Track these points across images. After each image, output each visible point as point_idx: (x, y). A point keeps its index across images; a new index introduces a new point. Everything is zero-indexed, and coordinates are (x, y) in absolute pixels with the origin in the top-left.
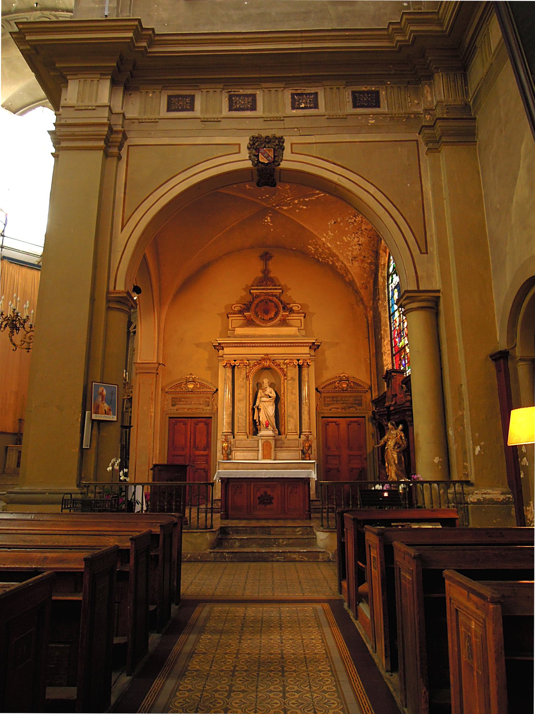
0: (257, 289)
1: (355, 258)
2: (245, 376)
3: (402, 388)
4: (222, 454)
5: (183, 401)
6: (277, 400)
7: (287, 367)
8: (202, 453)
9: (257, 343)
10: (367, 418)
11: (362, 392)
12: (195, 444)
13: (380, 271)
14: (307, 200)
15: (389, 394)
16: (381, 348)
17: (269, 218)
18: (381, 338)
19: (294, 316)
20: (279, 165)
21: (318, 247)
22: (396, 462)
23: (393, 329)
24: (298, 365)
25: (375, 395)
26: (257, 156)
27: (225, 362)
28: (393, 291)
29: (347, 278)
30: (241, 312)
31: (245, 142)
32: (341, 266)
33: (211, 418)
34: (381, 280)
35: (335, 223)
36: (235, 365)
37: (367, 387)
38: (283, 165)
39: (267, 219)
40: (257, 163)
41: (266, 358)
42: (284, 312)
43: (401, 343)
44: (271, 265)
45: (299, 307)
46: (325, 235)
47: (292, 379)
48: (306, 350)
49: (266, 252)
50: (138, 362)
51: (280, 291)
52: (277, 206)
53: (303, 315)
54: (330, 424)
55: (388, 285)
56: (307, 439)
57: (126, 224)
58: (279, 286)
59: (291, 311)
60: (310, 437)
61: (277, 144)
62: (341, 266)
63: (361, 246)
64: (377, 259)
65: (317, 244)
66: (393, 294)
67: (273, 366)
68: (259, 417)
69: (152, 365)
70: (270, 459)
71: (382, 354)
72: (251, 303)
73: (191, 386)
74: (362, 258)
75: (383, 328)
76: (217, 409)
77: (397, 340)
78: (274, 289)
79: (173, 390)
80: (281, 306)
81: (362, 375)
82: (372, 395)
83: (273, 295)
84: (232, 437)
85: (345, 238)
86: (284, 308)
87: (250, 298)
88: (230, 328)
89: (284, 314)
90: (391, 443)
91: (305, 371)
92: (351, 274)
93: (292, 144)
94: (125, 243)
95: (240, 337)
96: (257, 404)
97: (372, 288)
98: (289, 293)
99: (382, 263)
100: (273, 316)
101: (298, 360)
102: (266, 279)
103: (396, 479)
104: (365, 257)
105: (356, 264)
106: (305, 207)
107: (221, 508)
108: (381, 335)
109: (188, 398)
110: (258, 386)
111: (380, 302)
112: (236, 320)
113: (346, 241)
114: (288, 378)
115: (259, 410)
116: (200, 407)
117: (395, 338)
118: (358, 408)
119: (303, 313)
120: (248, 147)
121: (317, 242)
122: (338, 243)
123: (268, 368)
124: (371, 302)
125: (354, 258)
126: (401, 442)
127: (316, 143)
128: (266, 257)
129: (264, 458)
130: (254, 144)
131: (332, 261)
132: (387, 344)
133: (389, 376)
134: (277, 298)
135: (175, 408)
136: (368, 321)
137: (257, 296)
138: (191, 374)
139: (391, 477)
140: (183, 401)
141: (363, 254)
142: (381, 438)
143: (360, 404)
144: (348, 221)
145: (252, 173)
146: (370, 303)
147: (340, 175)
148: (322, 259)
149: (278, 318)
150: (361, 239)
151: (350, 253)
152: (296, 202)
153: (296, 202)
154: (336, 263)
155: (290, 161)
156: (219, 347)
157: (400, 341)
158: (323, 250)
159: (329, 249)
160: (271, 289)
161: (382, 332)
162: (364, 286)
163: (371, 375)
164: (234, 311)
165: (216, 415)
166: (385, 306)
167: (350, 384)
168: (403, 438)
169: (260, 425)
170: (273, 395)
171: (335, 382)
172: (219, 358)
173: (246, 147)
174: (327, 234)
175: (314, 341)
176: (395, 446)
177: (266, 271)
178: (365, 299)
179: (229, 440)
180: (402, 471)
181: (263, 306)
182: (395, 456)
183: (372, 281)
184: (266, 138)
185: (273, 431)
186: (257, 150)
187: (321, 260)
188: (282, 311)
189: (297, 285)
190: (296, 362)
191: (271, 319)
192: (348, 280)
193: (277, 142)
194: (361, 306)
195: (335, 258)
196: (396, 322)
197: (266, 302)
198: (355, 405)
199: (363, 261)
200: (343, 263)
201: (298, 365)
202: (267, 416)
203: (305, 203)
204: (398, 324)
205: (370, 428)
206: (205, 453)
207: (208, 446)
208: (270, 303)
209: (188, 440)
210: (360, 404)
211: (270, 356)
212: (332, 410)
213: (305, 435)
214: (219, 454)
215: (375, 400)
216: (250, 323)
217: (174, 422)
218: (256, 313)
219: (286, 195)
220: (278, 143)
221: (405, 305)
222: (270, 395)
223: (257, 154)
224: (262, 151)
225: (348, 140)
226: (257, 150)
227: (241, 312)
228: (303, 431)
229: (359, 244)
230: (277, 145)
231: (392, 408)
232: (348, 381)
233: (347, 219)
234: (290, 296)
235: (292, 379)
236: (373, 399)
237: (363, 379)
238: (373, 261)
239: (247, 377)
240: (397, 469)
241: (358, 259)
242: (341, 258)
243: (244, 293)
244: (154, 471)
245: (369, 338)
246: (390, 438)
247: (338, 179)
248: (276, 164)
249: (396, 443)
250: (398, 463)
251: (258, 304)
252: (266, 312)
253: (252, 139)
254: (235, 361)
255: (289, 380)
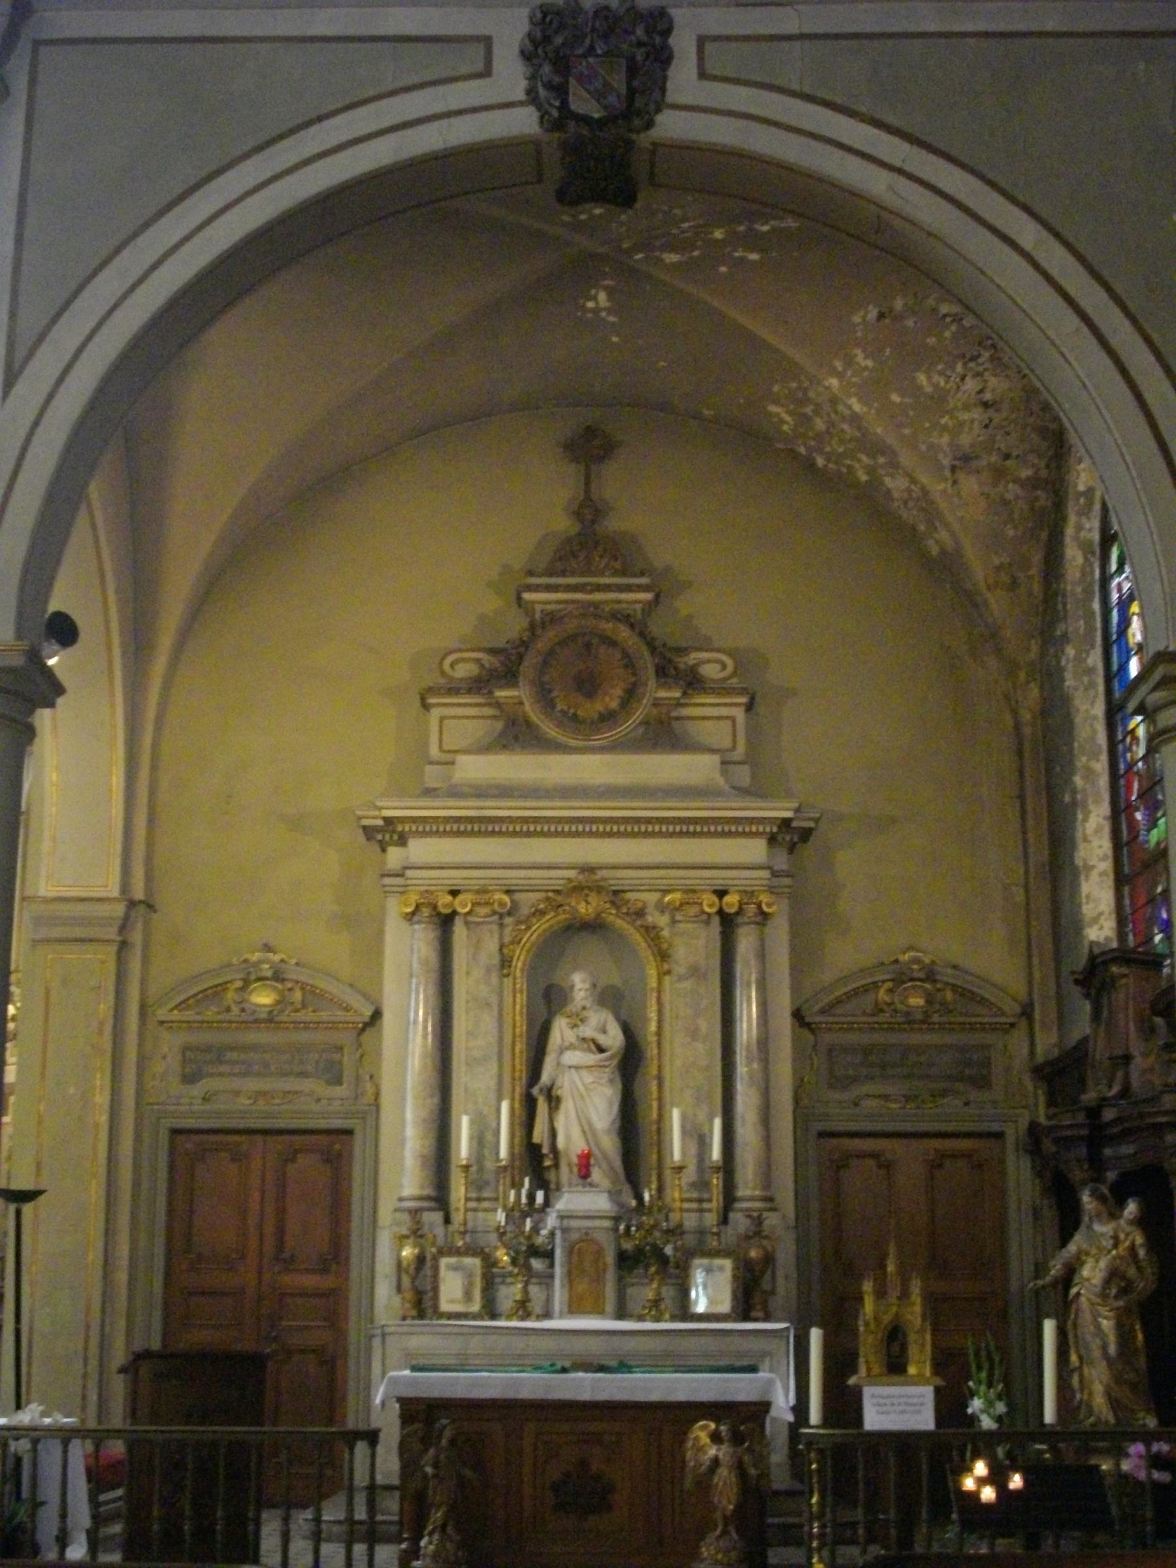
0: (549, 588)
1: (966, 459)
2: (496, 961)
3: (1153, 1030)
4: (399, 1289)
5: (233, 1063)
6: (630, 1063)
7: (674, 922)
8: (310, 1281)
9: (548, 820)
10: (1010, 1140)
11: (994, 1028)
12: (280, 1245)
13: (1072, 519)
14: (765, 228)
15: (1100, 1051)
16: (1073, 846)
17: (602, 296)
18: (1074, 803)
19: (703, 707)
20: (650, 124)
21: (808, 410)
22: (1112, 1350)
23: (1122, 766)
24: (721, 912)
25: (1047, 1044)
26: (561, 91)
27: (414, 898)
28: (1124, 605)
29: (931, 542)
30: (480, 685)
31: (510, 29)
32: (909, 491)
33: (349, 1132)
34: (1073, 556)
35: (881, 316)
36: (455, 913)
37: (1012, 1008)
38: (670, 126)
39: (595, 298)
40: (559, 119)
41: (589, 880)
42: (661, 686)
43: (1155, 832)
44: (613, 481)
45: (724, 667)
46: (838, 365)
47: (695, 972)
48: (755, 850)
49: (588, 428)
50: (42, 892)
51: (647, 596)
52: (635, 249)
53: (743, 700)
54: (854, 1162)
55: (1105, 580)
56: (757, 1231)
57: (21, 372)
58: (642, 574)
59: (693, 682)
60: (772, 1220)
61: (646, 51)
62: (909, 491)
63: (991, 412)
64: (1059, 468)
65: (806, 400)
66: (1125, 622)
67: (611, 917)
68: (553, 1134)
69: (103, 910)
70: (599, 1312)
71: (1076, 873)
72: (524, 645)
73: (263, 998)
74: (993, 459)
75: (1082, 761)
76: (377, 1095)
77: (1139, 816)
78: (620, 589)
79: (189, 1015)
80: (648, 663)
81: (994, 960)
82: (1032, 1044)
83: (615, 616)
84: (438, 1217)
85: (922, 378)
86: (662, 672)
87: (515, 626)
88: (434, 751)
89: (662, 694)
90: (1092, 1273)
91: (746, 942)
92: (947, 525)
93: (702, 41)
94: (19, 444)
95: (479, 796)
96: (545, 1078)
97: (1037, 587)
98: (684, 605)
99: (1081, 488)
100: (614, 704)
101: (721, 894)
102: (589, 543)
103: (1112, 1420)
104: (1007, 457)
105: (970, 484)
106: (754, 257)
107: (401, 1523)
108: (1074, 792)
109: (254, 1048)
110: (549, 1001)
111: (1070, 651)
112: (463, 720)
113: (929, 389)
114: (680, 970)
115: (554, 1102)
116: (308, 1085)
117: (1130, 808)
118: (974, 1095)
119: (743, 691)
120: (522, 52)
121: (805, 391)
122: (895, 398)
123: (593, 926)
124: (1035, 648)
125: (964, 461)
126: (1132, 1272)
127: (801, 37)
128: (590, 448)
129: (575, 1307)
130: (547, 39)
131: (871, 470)
132: (1098, 831)
133: (1096, 975)
134: (632, 626)
135: (198, 1090)
136: (1017, 727)
137: (552, 619)
138: (268, 948)
139: (1090, 1412)
140: (233, 1063)
141: (1002, 443)
142: (1064, 1241)
143: (982, 1082)
144: (934, 310)
145: (539, 152)
146: (1028, 650)
147: (900, 171)
148: (828, 460)
149: (638, 715)
150: (993, 382)
151: (945, 439)
152: (718, 234)
153: (718, 234)
154: (887, 480)
155: (695, 111)
156: (390, 833)
157: (1153, 824)
158: (831, 424)
159: (855, 419)
160: (608, 588)
161: (1078, 780)
162: (1005, 578)
163: (1030, 957)
164: (451, 679)
165: (370, 1121)
166: (1091, 671)
167: (939, 995)
168: (1142, 1253)
169: (556, 1165)
170: (614, 1038)
171: (875, 985)
172: (387, 881)
173: (516, 51)
174: (849, 361)
175: (788, 814)
176: (1107, 1282)
177: (589, 511)
178: (1008, 633)
179: (426, 1229)
180: (1133, 1386)
181: (581, 662)
182: (1107, 1324)
183: (1037, 558)
184: (596, 13)
185: (614, 1195)
186: (562, 64)
187: (820, 461)
188: (652, 682)
189: (727, 572)
190: (709, 904)
191: (608, 718)
192: (935, 551)
193: (640, 32)
194: (992, 662)
195: (881, 460)
196: (1135, 739)
197: (586, 643)
198: (960, 1086)
199: (999, 474)
200: (913, 481)
201: (721, 912)
202: (588, 1131)
203: (753, 241)
204: (1141, 751)
205: (1020, 1178)
206: (326, 1282)
207: (336, 1254)
208: (602, 650)
209: (252, 1221)
210: (982, 1082)
211: (601, 874)
212: (864, 1103)
213: (748, 1213)
214: (384, 1293)
215: (1049, 1063)
216: (516, 734)
217: (192, 1152)
218: (546, 699)
219: (677, 211)
220: (644, 38)
221: (1159, 708)
222: (602, 1040)
223: (557, 80)
224: (582, 67)
225: (932, 28)
226: (562, 64)
227: (480, 685)
228: (740, 1193)
229: (986, 405)
230: (640, 44)
231: (1109, 1114)
232: (935, 981)
233: (931, 302)
234: (690, 617)
235: (695, 972)
236: (1040, 1059)
237: (997, 978)
238: (1044, 473)
239: (505, 963)
240: (1118, 1379)
241: (974, 464)
242: (906, 459)
243: (491, 604)
244: (135, 1381)
245: (1022, 798)
246: (1087, 1254)
247: (891, 188)
248: (637, 122)
249: (1113, 1275)
250: (1120, 1354)
251: (551, 653)
252: (588, 685)
253: (539, 15)
254: (454, 893)
255: (680, 979)
